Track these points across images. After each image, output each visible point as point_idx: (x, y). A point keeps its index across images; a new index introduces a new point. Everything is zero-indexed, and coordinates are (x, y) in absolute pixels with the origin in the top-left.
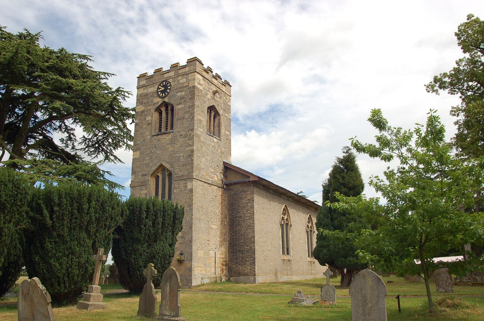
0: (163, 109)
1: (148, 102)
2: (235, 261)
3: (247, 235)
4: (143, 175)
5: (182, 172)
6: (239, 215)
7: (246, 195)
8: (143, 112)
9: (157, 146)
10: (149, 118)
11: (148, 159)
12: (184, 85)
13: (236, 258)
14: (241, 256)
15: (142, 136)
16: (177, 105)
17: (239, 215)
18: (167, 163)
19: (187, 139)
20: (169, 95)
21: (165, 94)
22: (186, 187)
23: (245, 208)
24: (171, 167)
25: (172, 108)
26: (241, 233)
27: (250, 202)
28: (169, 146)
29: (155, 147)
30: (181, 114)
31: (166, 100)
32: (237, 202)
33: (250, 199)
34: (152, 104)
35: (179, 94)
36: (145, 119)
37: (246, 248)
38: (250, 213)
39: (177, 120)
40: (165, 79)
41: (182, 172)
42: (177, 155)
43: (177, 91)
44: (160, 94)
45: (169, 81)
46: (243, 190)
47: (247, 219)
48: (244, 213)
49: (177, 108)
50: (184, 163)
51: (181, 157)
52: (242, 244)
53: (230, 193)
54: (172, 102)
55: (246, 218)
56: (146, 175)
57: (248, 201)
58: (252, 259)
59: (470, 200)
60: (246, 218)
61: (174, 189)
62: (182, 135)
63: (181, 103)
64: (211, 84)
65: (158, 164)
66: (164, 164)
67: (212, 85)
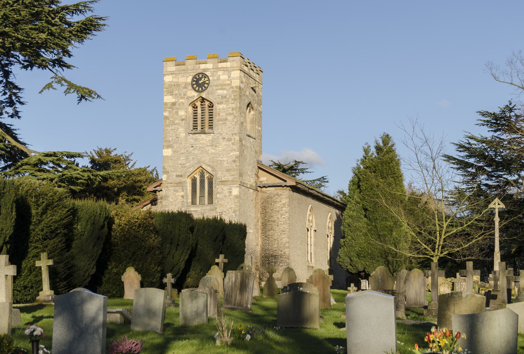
0: (198, 104)
1: (180, 94)
2: (267, 266)
3: (281, 240)
4: (177, 176)
5: (226, 177)
6: (272, 219)
7: (281, 199)
8: (174, 104)
9: (195, 146)
10: (182, 113)
11: (184, 158)
12: (226, 83)
13: (269, 263)
14: (274, 261)
15: (174, 132)
16: (218, 104)
17: (272, 219)
18: (209, 165)
19: (231, 143)
20: (206, 91)
21: (202, 89)
22: (231, 192)
23: (279, 213)
24: (213, 171)
25: (211, 105)
26: (274, 238)
27: (285, 206)
28: (209, 148)
29: (192, 147)
30: (223, 114)
31: (204, 95)
32: (270, 206)
33: (284, 204)
34: (186, 97)
35: (220, 92)
36: (177, 113)
37: (280, 253)
38: (284, 218)
39: (219, 120)
40: (201, 71)
41: (226, 177)
42: (220, 159)
43: (217, 88)
44: (196, 87)
45: (207, 73)
46: (278, 193)
47: (281, 224)
48: (278, 218)
49: (217, 107)
50: (228, 168)
51: (224, 161)
52: (275, 249)
53: (262, 196)
54: (211, 99)
55: (280, 223)
56: (181, 176)
57: (282, 205)
58: (286, 264)
59: (489, 153)
60: (280, 223)
61: (217, 194)
62: (225, 138)
63: (223, 103)
64: (249, 77)
65: (197, 166)
66: (204, 167)
67: (251, 78)
